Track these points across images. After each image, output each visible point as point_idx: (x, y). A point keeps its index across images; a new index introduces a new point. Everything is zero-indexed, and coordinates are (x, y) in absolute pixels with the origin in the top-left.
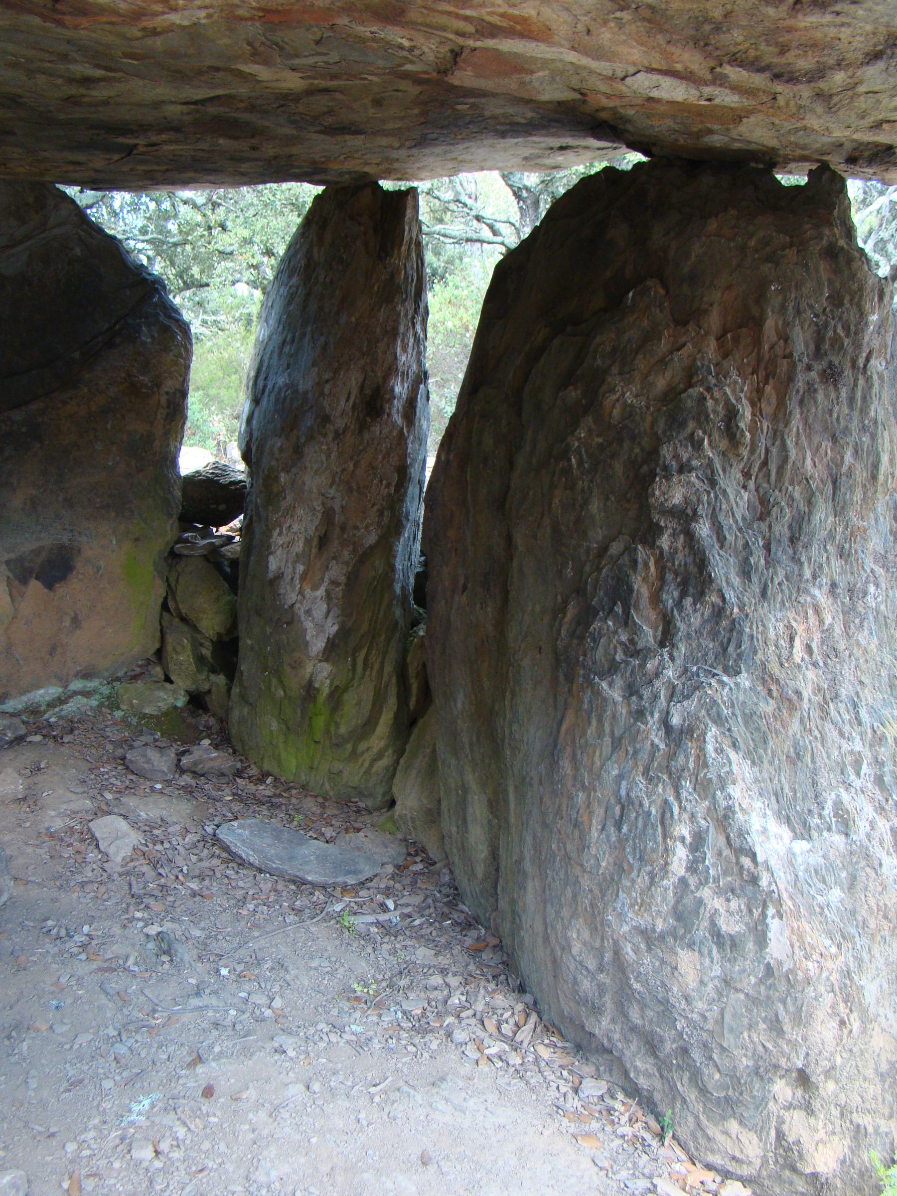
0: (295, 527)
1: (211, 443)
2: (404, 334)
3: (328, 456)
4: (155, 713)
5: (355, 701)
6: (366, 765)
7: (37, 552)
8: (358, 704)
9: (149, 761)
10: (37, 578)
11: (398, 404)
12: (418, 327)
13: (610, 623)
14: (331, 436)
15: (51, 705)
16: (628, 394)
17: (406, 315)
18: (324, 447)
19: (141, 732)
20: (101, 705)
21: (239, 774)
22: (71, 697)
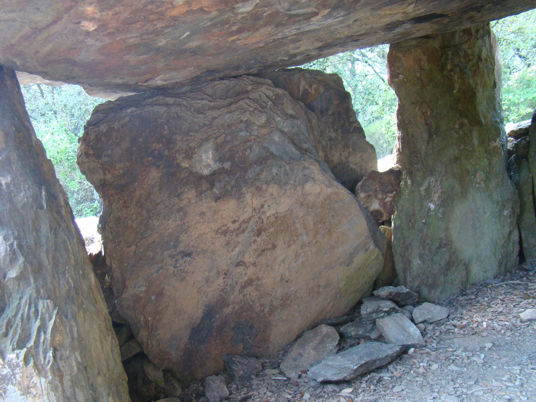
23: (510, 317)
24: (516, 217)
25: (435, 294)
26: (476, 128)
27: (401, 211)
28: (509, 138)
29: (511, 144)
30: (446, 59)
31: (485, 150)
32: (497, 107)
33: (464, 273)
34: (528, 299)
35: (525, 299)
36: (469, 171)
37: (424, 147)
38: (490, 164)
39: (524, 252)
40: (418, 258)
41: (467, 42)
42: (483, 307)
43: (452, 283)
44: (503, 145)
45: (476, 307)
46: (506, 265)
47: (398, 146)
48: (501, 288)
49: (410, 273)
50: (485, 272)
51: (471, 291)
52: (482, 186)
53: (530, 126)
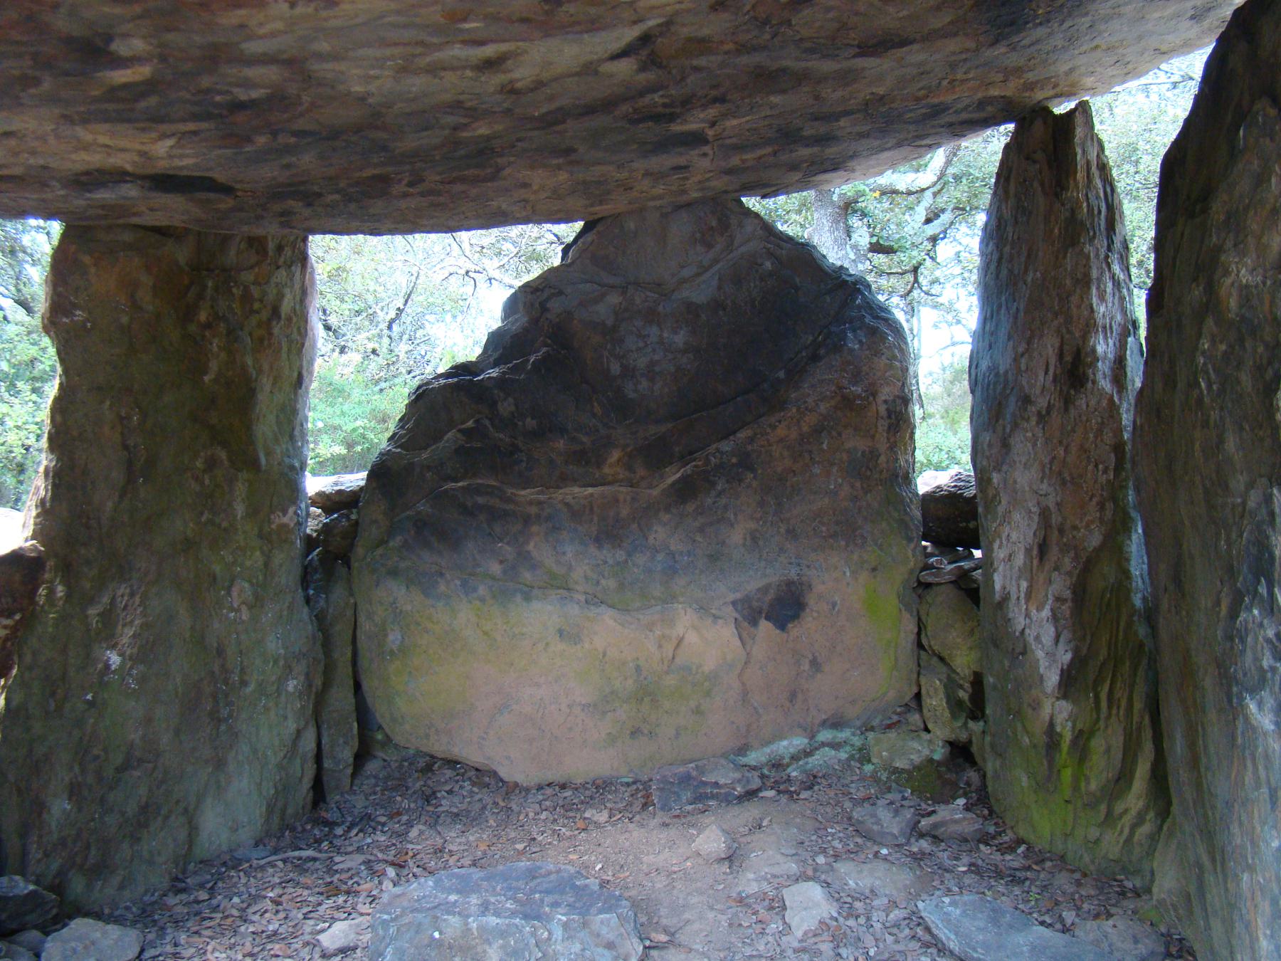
0: (1014, 536)
1: (942, 451)
2: (1099, 280)
3: (1034, 445)
4: (907, 767)
5: (1102, 749)
6: (1126, 831)
7: (765, 590)
8: (1108, 750)
9: (878, 822)
10: (767, 618)
11: (1103, 367)
12: (1116, 268)
13: (1256, 612)
14: (1034, 420)
15: (795, 758)
16: (1243, 271)
17: (1097, 255)
18: (1029, 434)
19: (889, 790)
20: (852, 757)
21: (985, 839)
22: (817, 749)
23: (297, 944)
24: (313, 697)
25: (104, 891)
26: (244, 475)
27: (30, 668)
28: (313, 509)
29: (315, 521)
30: (200, 297)
31: (261, 530)
32: (297, 433)
33: (182, 835)
34: (336, 895)
35: (328, 898)
36: (215, 578)
37: (110, 505)
38: (266, 565)
39: (325, 778)
40: (65, 796)
41: (252, 267)
42: (229, 921)
43: (151, 862)
44: (299, 524)
45: (212, 924)
46: (283, 811)
47: (42, 493)
48: (271, 870)
49: (40, 837)
50: (234, 830)
51: (198, 879)
52: (244, 618)
53: (362, 489)
